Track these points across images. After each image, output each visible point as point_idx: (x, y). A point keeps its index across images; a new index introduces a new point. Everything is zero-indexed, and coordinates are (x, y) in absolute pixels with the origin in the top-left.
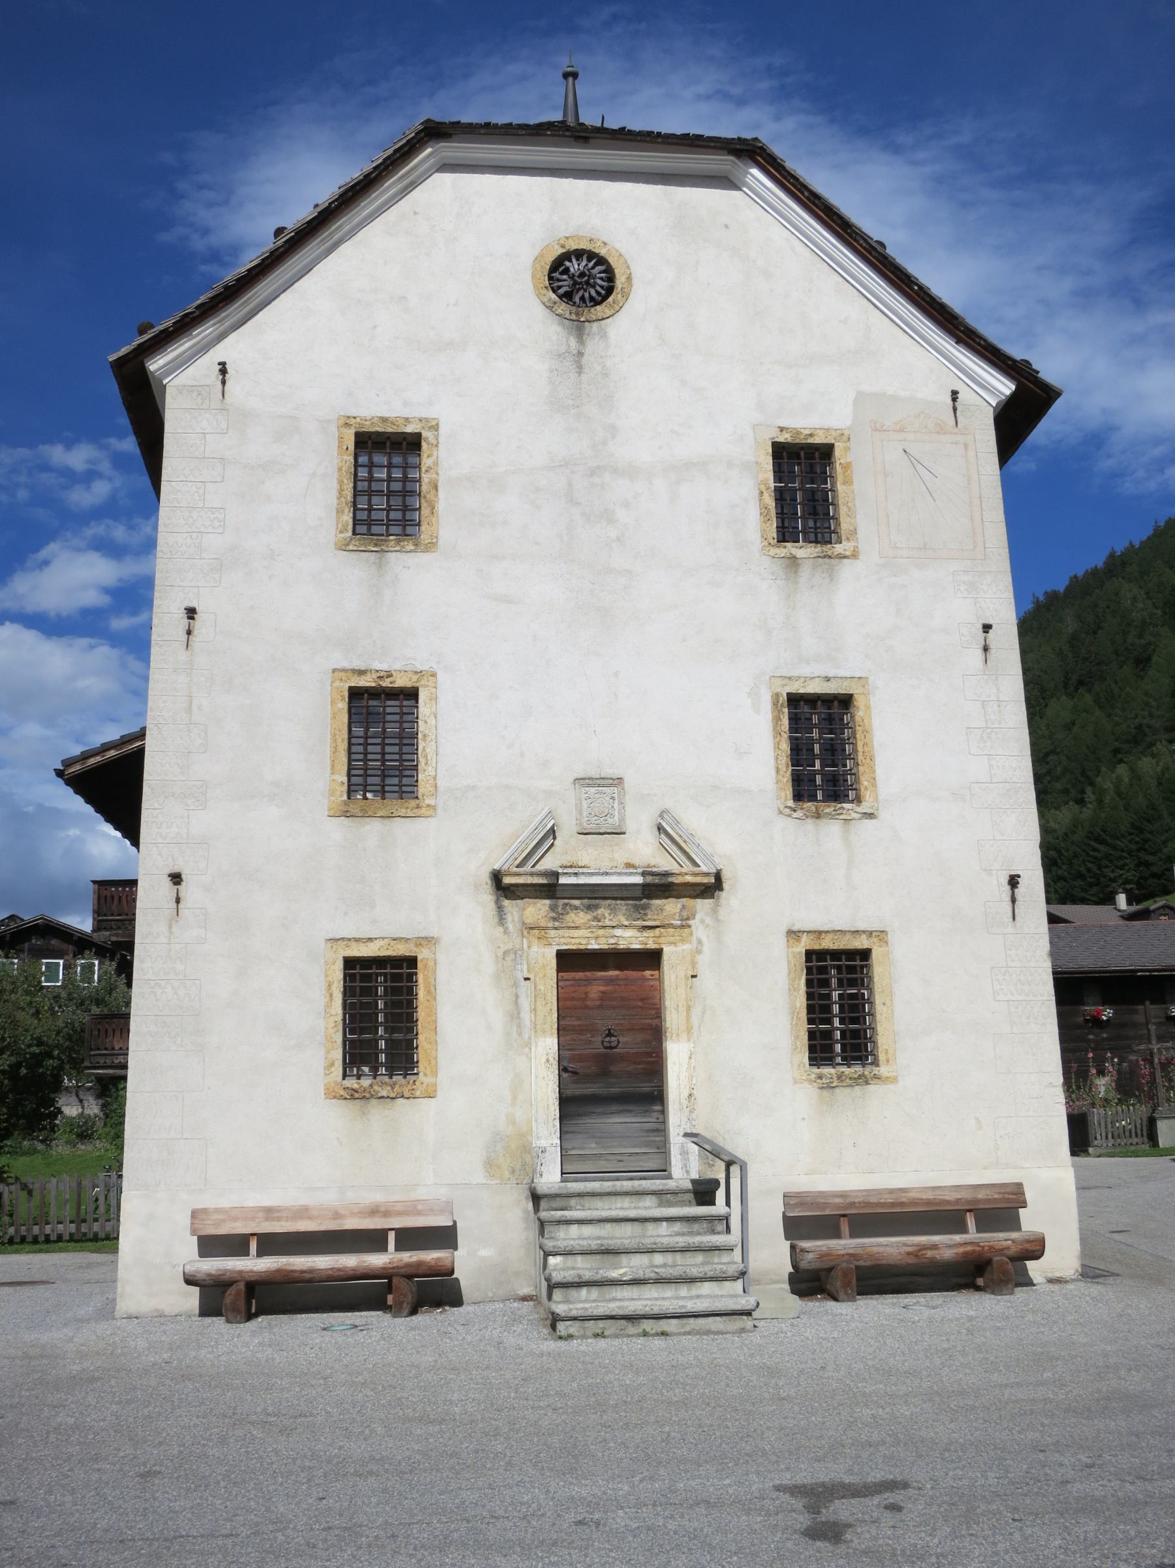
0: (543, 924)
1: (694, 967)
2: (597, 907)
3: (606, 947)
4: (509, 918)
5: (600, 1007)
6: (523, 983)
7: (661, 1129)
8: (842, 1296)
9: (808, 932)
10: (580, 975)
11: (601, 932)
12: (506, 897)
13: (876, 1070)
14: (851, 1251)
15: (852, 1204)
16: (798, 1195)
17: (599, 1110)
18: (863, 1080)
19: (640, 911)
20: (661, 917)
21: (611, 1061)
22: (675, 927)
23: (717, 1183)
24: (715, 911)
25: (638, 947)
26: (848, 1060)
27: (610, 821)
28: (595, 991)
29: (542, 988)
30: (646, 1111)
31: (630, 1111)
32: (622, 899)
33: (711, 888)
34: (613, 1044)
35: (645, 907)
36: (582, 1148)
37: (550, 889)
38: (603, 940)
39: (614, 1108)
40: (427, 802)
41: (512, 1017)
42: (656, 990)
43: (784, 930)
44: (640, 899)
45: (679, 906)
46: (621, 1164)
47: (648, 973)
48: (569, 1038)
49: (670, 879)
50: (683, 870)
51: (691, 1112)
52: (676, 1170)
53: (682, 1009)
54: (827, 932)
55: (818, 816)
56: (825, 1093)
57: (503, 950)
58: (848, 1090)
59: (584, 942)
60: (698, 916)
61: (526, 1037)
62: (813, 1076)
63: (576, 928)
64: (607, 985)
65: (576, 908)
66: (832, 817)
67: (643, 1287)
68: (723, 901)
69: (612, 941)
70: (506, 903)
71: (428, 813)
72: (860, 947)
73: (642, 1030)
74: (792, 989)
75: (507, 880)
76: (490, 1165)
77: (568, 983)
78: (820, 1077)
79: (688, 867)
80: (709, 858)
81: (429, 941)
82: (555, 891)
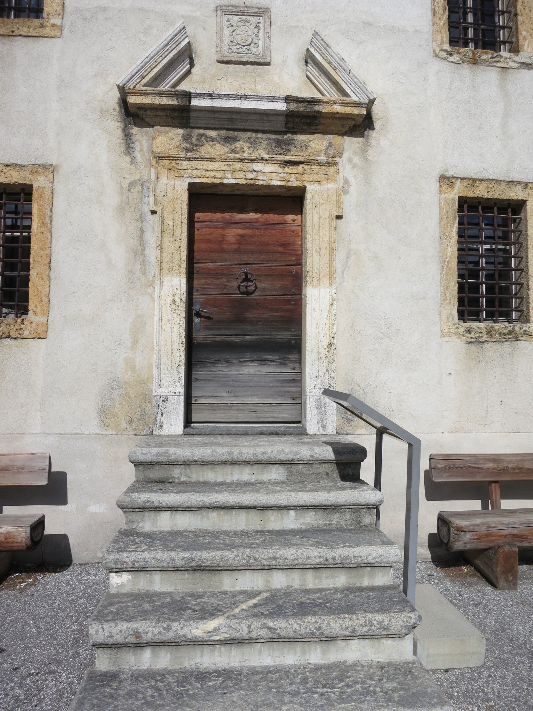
0: (174, 153)
1: (339, 207)
2: (235, 139)
3: (244, 182)
4: (137, 147)
5: (237, 251)
6: (150, 216)
7: (297, 380)
8: (502, 583)
9: (462, 179)
10: (218, 216)
11: (238, 166)
12: (136, 125)
13: (526, 327)
14: (515, 532)
15: (504, 471)
16: (446, 458)
17: (233, 357)
18: (513, 336)
19: (283, 146)
20: (305, 153)
21: (244, 301)
22: (320, 164)
23: (362, 453)
24: (364, 151)
25: (278, 183)
26: (492, 316)
27: (253, 50)
28: (232, 234)
29: (171, 223)
30: (283, 360)
31: (265, 360)
32: (263, 132)
33: (360, 124)
34: (251, 289)
35: (289, 143)
36: (213, 397)
37: (181, 114)
38: (241, 175)
39: (248, 356)
40: (52, 21)
41: (135, 253)
42: (297, 235)
43: (436, 175)
44: (285, 133)
45: (325, 143)
46: (253, 414)
47: (289, 217)
48: (203, 281)
49: (317, 108)
50: (332, 99)
51: (331, 362)
52: (312, 426)
53: (325, 252)
54: (482, 180)
55: (475, 62)
56: (474, 348)
57: (128, 181)
58: (497, 346)
59: (219, 175)
60: (346, 155)
61: (150, 274)
62: (462, 330)
63: (211, 160)
64: (246, 228)
65: (213, 140)
66: (489, 64)
67: (246, 649)
68: (373, 142)
69: (251, 176)
70: (135, 130)
71: (53, 33)
72: (515, 198)
73: (282, 276)
74: (443, 237)
75: (132, 100)
76: (105, 414)
77: (204, 224)
78: (469, 331)
79: (335, 96)
80: (361, 86)
81: (48, 169)
82: (188, 118)
